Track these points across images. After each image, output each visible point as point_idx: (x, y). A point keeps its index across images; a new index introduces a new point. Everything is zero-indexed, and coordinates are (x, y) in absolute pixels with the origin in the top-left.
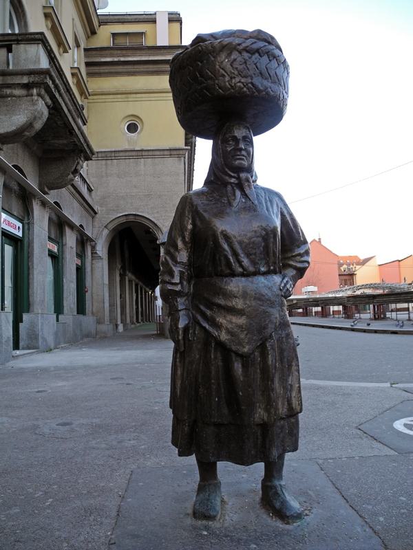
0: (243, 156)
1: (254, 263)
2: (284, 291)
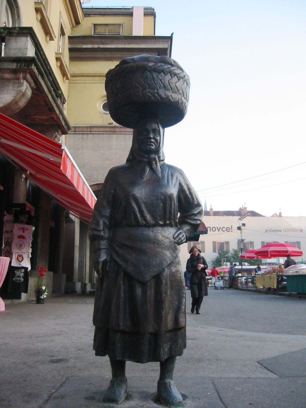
1: (154, 217)
2: (177, 239)
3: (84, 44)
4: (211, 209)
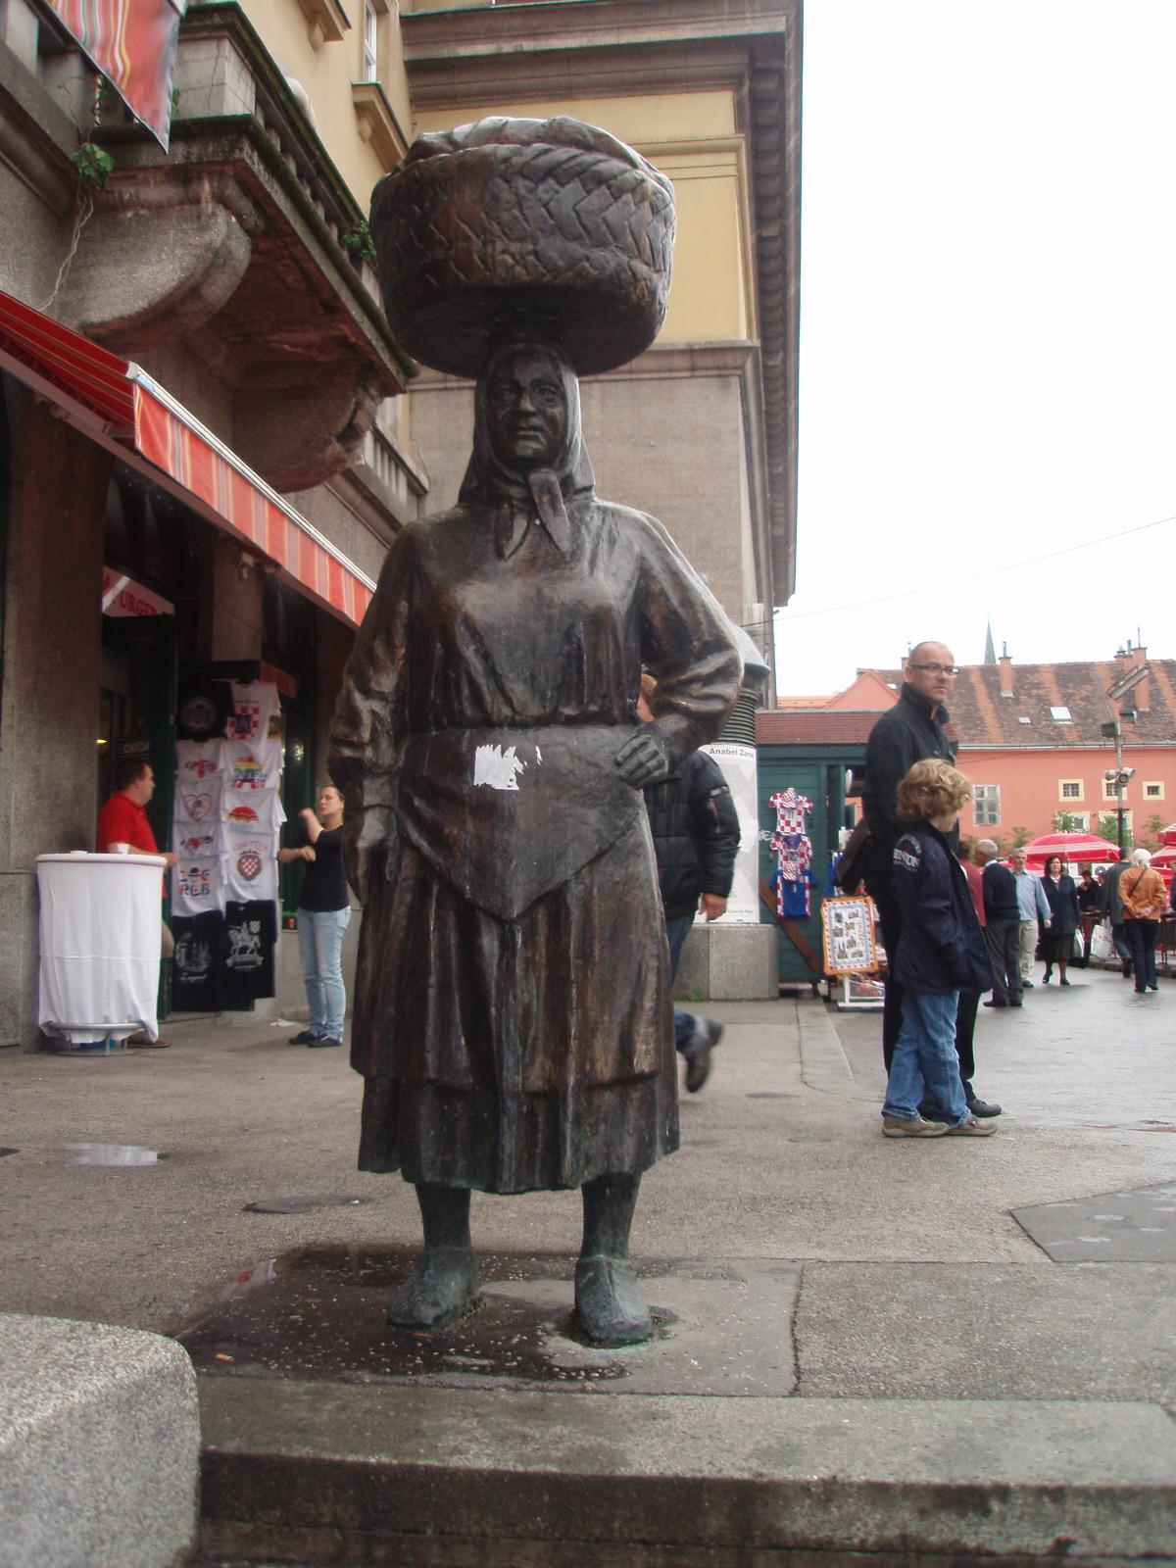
3: (465, 40)
4: (1006, 658)
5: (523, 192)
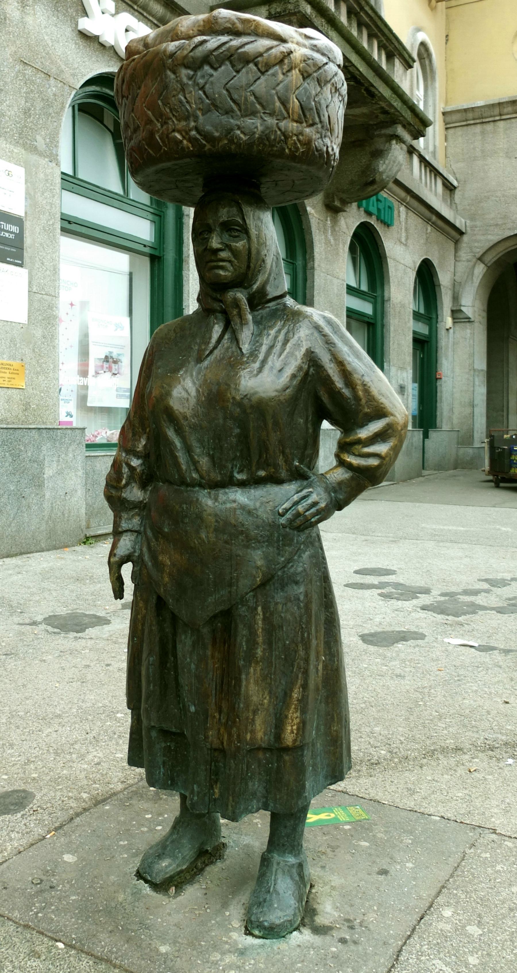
0: (223, 260)
5: (185, 80)
